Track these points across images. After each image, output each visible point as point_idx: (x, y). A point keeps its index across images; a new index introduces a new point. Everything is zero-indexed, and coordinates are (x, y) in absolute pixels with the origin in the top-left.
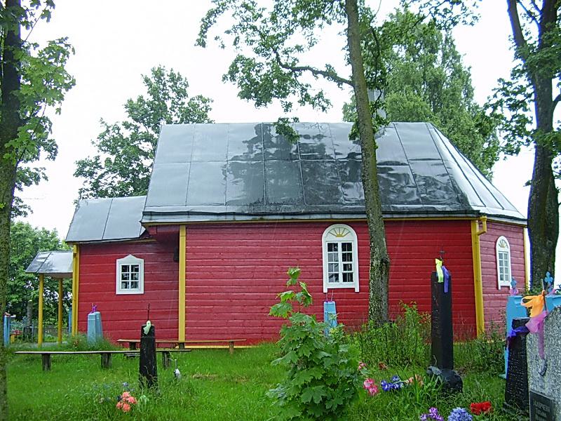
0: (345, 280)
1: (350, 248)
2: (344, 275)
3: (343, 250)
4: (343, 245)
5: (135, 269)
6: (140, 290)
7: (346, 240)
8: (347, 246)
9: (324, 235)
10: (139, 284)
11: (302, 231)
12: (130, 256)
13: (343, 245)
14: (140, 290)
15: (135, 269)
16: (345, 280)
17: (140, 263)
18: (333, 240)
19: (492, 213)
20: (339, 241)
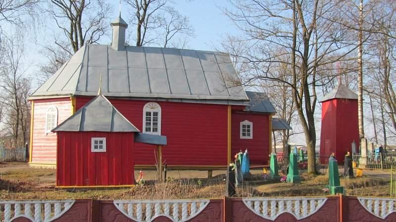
0: (153, 131)
1: (243, 134)
2: (153, 129)
3: (154, 115)
4: (154, 113)
5: (249, 126)
6: (251, 137)
7: (155, 110)
8: (156, 114)
9: (144, 108)
10: (145, 114)
11: (47, 103)
12: (246, 121)
13: (154, 113)
14: (251, 137)
15: (249, 126)
16: (153, 131)
17: (251, 124)
18: (149, 110)
19: (63, 121)
20: (152, 111)
